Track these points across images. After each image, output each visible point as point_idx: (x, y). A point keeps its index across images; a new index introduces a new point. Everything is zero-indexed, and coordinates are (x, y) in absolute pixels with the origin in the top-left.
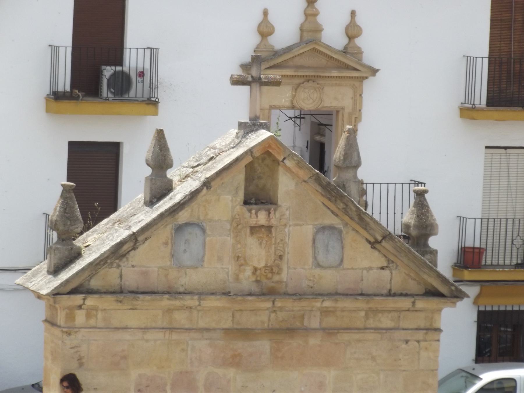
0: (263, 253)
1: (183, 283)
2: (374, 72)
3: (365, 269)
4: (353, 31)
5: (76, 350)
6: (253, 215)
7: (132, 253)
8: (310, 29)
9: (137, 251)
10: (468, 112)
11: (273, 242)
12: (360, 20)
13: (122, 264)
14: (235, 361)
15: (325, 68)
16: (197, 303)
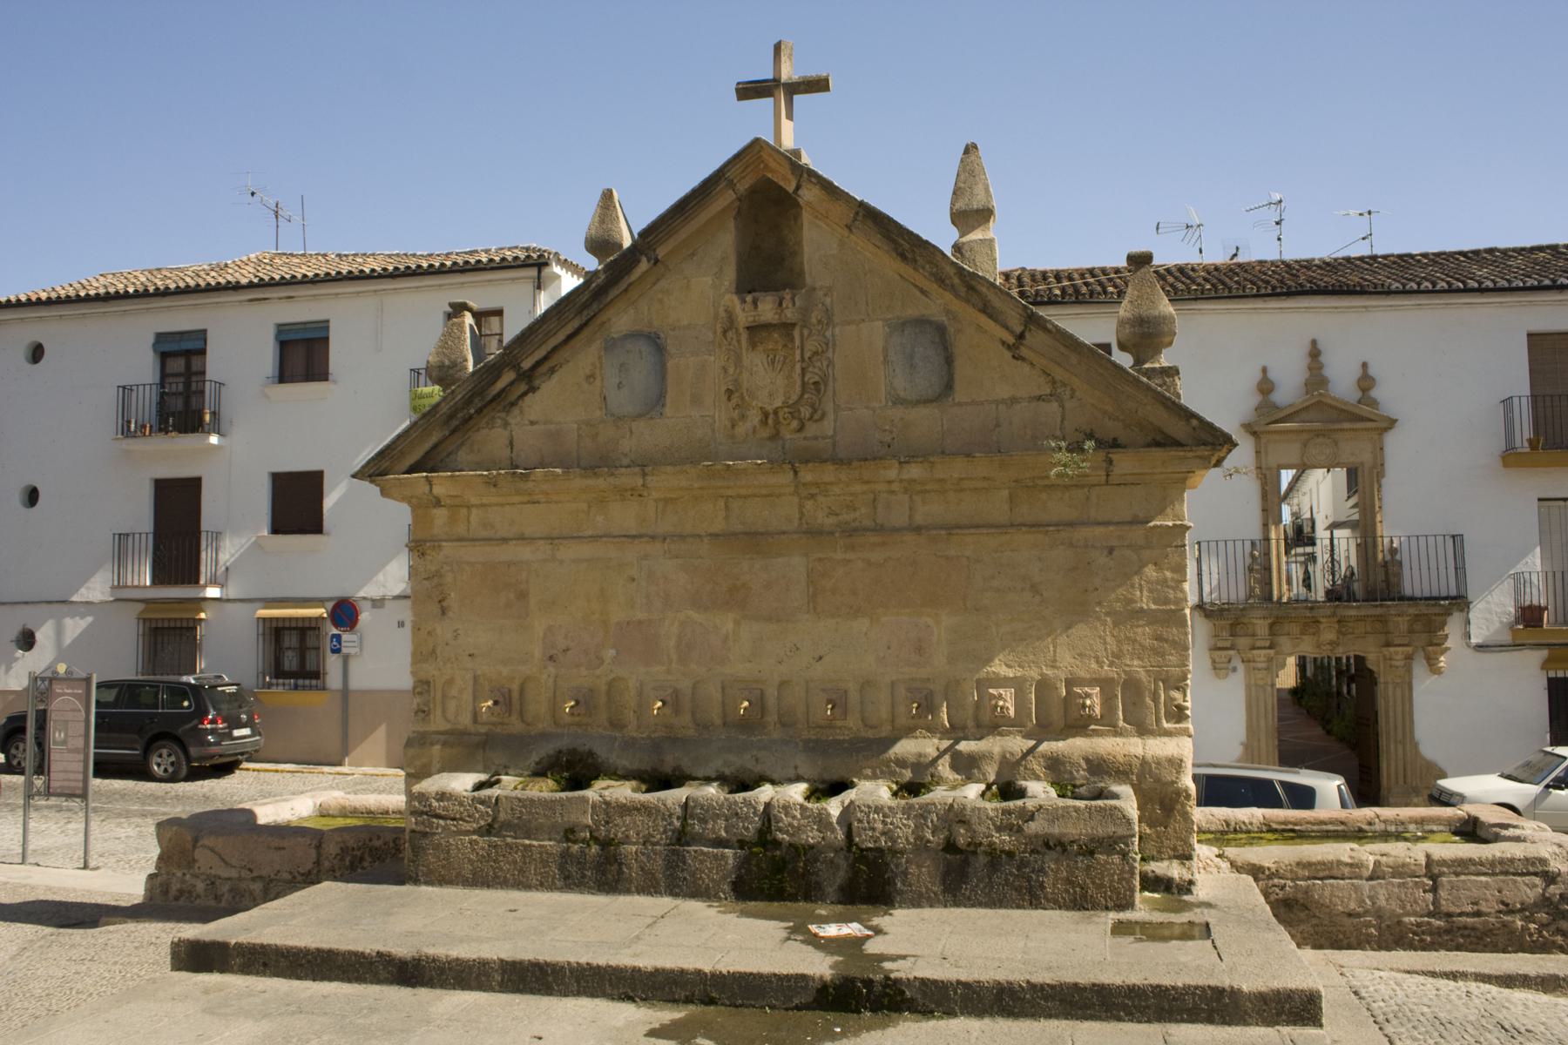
0: (780, 381)
1: (626, 450)
2: (1391, 423)
3: (1003, 401)
4: (1366, 381)
5: (436, 580)
6: (749, 306)
7: (529, 398)
8: (1316, 376)
9: (538, 393)
10: (1510, 458)
11: (798, 357)
12: (1372, 371)
13: (512, 421)
14: (735, 598)
15: (1339, 421)
16: (640, 482)
